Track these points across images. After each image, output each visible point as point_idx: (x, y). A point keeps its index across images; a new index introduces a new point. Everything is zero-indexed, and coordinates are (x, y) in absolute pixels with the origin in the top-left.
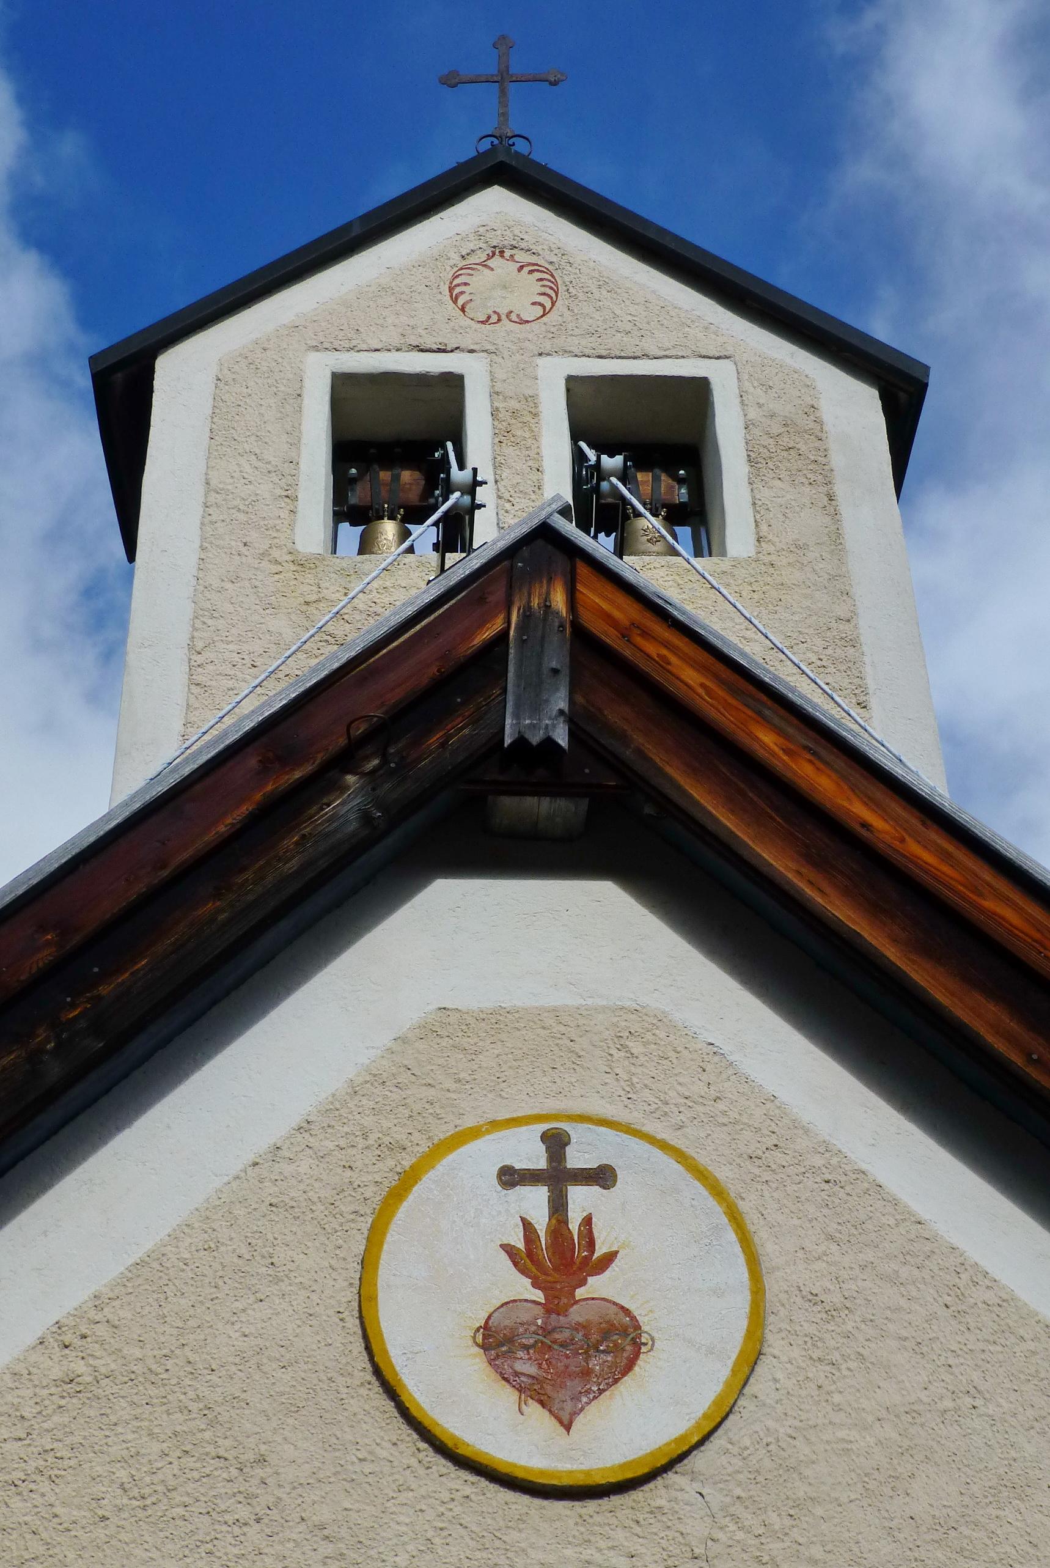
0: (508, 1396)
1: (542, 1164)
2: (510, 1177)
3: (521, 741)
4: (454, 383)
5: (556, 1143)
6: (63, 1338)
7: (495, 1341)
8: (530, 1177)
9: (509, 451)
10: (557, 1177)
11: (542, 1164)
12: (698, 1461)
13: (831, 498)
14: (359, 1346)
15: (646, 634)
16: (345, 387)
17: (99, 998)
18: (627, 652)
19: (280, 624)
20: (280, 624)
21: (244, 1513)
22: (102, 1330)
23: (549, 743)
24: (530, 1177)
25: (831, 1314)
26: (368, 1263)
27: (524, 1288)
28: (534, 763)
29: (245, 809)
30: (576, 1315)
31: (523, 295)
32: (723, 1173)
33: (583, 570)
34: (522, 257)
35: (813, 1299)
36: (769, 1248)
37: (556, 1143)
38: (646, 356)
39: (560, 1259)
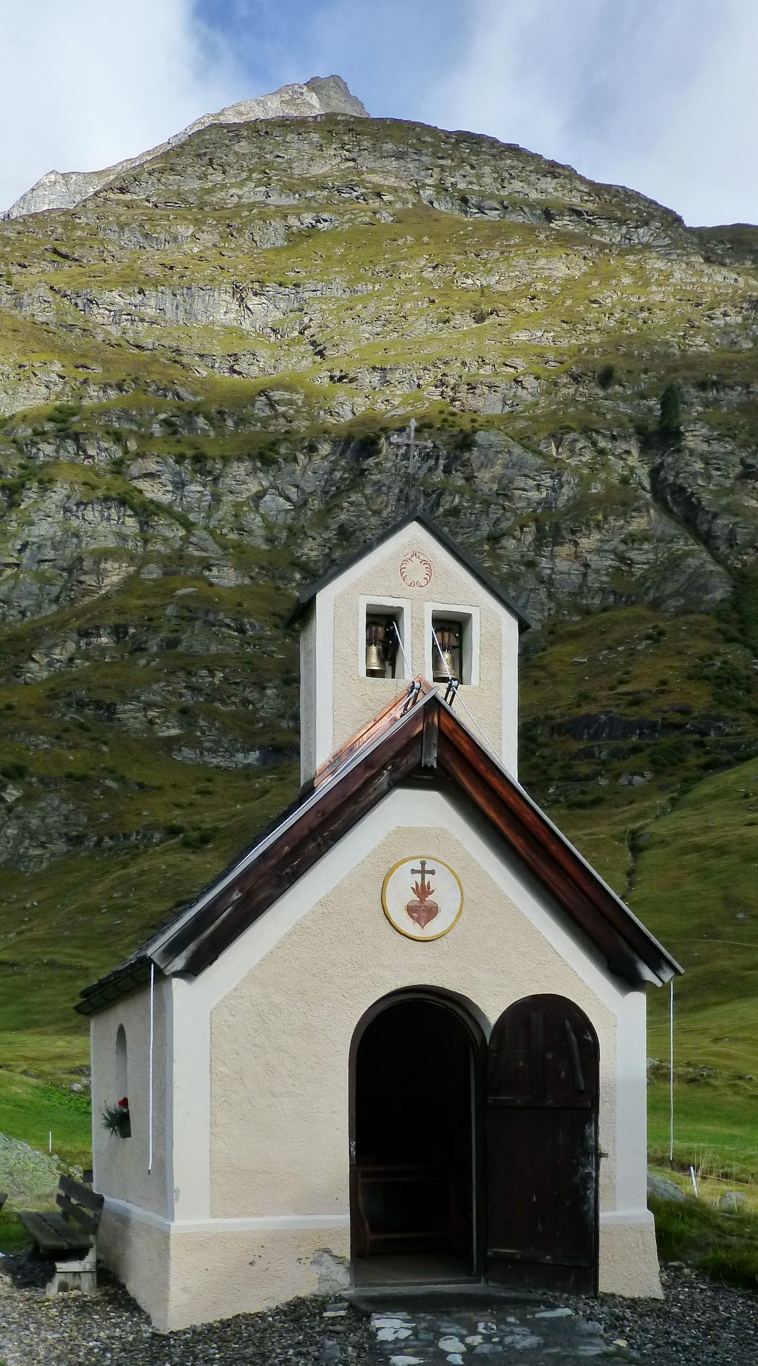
3: (426, 766)
5: (423, 864)
6: (321, 904)
7: (411, 910)
8: (418, 872)
10: (423, 872)
12: (447, 935)
14: (381, 908)
15: (456, 733)
18: (451, 738)
21: (359, 942)
23: (432, 766)
24: (418, 872)
28: (428, 770)
29: (362, 781)
30: (425, 904)
32: (457, 872)
33: (442, 710)
35: (473, 901)
36: (465, 890)
37: (423, 864)
39: (423, 891)
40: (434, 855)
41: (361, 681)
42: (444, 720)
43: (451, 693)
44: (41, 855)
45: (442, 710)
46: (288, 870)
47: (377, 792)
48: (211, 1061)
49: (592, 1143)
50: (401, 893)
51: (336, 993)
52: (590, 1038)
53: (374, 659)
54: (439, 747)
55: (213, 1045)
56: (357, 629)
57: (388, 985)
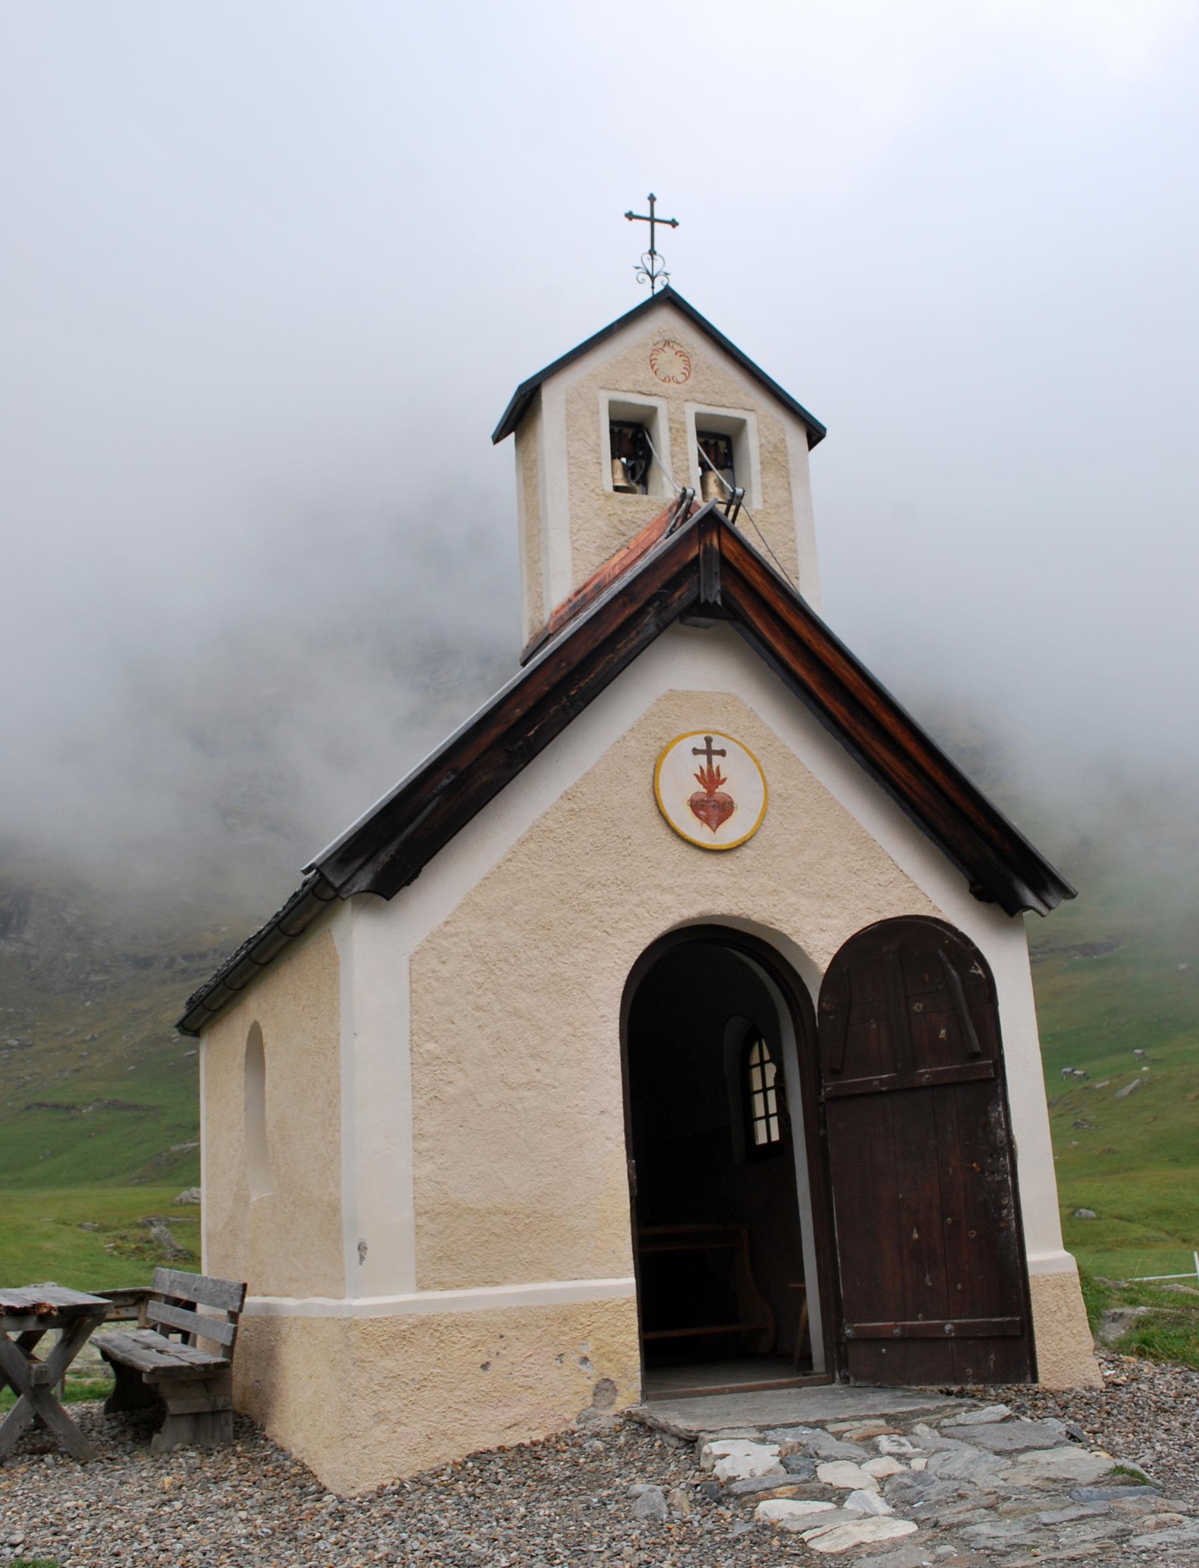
0: (698, 821)
1: (704, 748)
2: (696, 751)
3: (707, 602)
4: (653, 411)
5: (708, 741)
7: (696, 806)
9: (677, 449)
11: (704, 748)
12: (752, 844)
13: (789, 484)
16: (613, 405)
17: (580, 688)
18: (737, 566)
19: (600, 523)
20: (600, 523)
22: (579, 795)
23: (715, 602)
25: (784, 800)
26: (655, 778)
27: (701, 788)
31: (676, 368)
32: (755, 753)
33: (722, 531)
34: (677, 348)
35: (780, 795)
37: (708, 741)
38: (724, 406)
39: (711, 779)
40: (722, 729)
41: (608, 497)
42: (728, 544)
43: (733, 508)
44: (104, 981)
45: (722, 531)
46: (521, 743)
47: (641, 637)
48: (412, 1034)
49: (1001, 1133)
50: (680, 783)
51: (595, 927)
52: (980, 972)
53: (619, 475)
54: (722, 579)
55: (414, 1010)
56: (597, 431)
57: (670, 916)
